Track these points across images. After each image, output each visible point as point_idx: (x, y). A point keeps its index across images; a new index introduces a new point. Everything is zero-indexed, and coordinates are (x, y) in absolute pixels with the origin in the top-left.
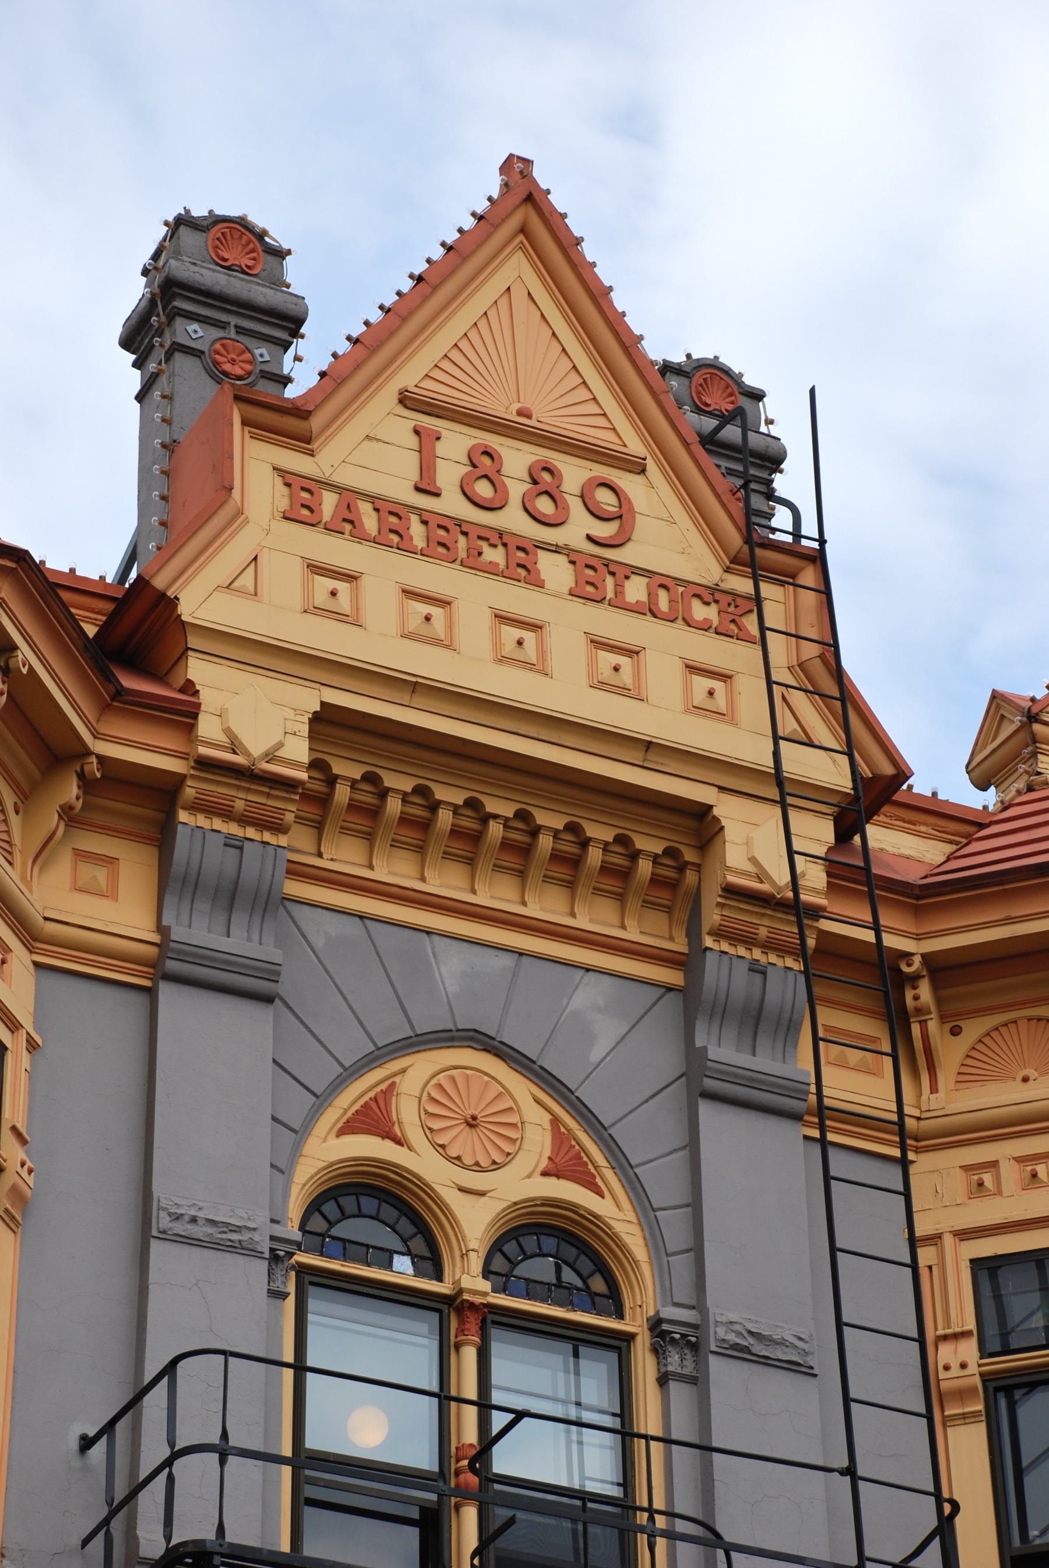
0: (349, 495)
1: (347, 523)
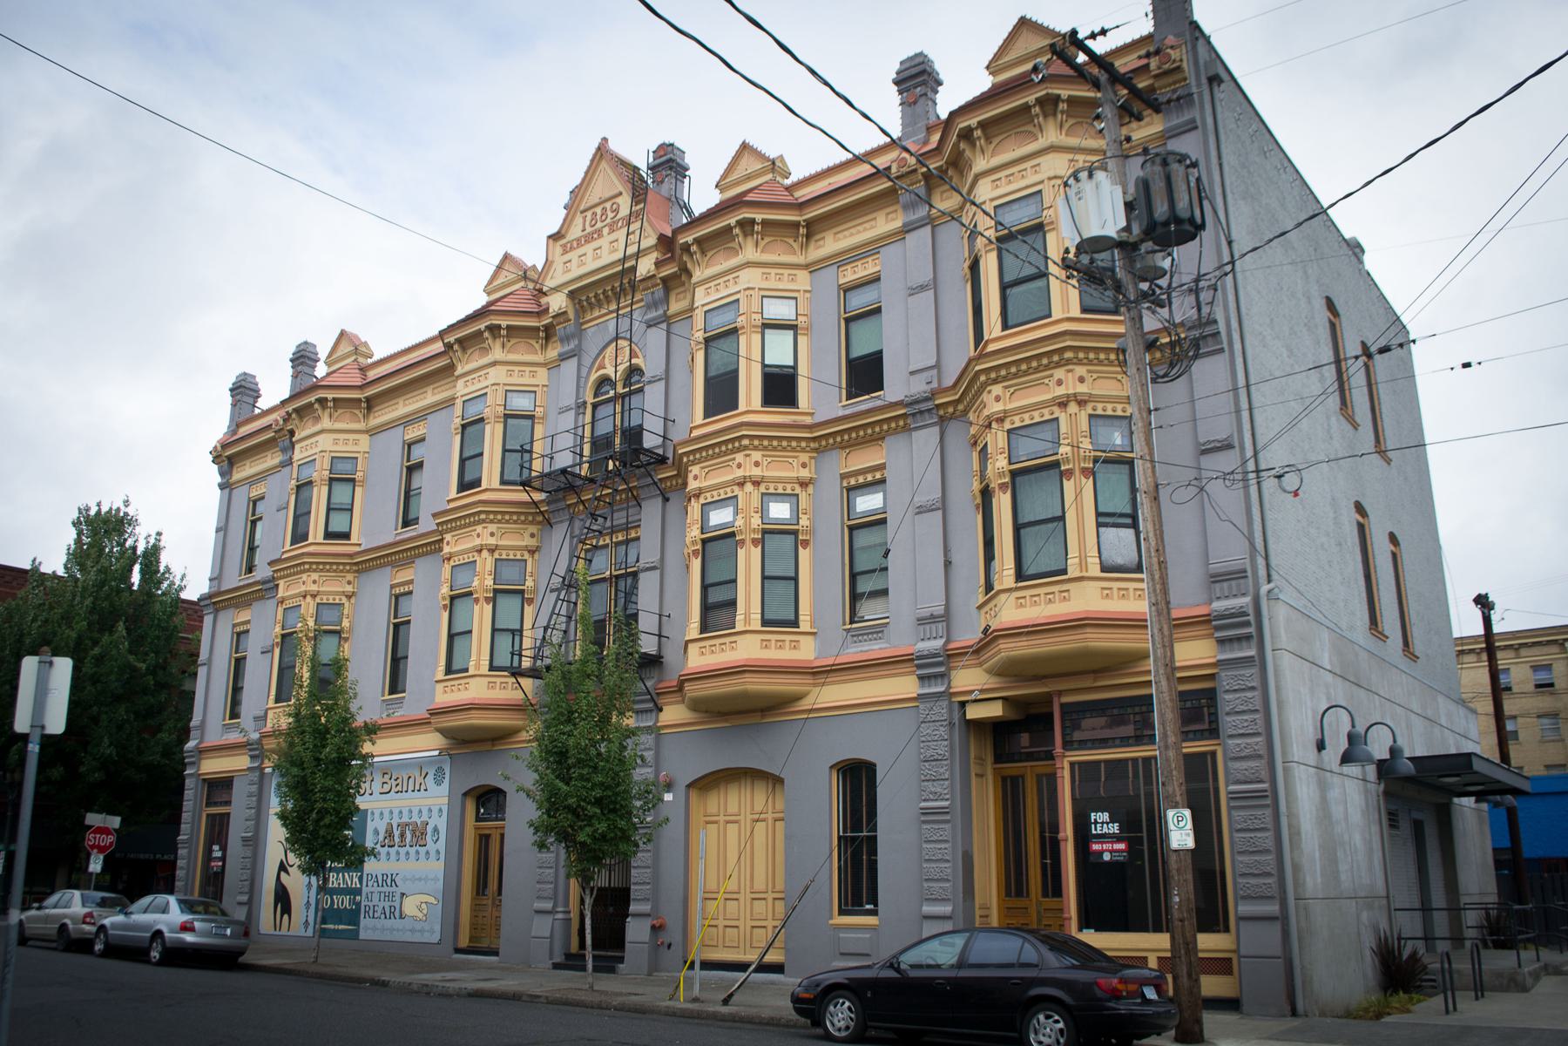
0: (578, 240)
1: (580, 245)
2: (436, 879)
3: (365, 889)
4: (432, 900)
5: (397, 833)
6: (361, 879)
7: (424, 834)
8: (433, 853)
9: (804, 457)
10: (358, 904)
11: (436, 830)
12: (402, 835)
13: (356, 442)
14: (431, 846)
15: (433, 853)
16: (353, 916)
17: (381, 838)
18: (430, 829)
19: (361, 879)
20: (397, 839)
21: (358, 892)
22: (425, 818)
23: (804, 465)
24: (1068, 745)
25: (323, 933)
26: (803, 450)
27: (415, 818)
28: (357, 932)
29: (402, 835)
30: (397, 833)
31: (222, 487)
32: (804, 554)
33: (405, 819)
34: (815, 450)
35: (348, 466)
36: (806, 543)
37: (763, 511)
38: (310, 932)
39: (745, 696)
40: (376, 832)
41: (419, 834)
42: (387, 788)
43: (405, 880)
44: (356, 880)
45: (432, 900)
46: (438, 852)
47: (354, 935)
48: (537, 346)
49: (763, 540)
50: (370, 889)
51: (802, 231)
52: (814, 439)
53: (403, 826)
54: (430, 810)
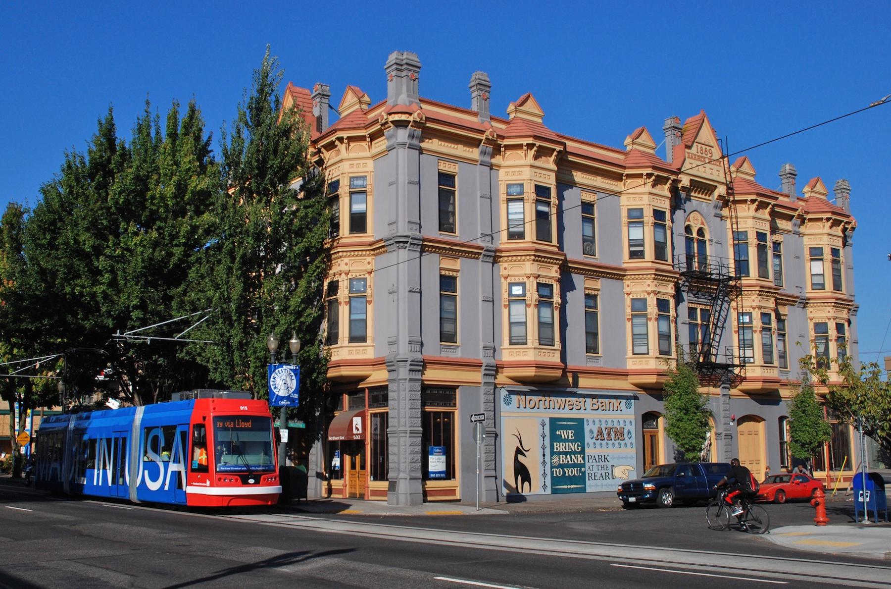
2: (632, 458)
3: (587, 465)
4: (631, 468)
5: (605, 433)
6: (584, 458)
7: (622, 434)
8: (629, 444)
9: (369, 259)
10: (584, 473)
11: (629, 432)
12: (609, 434)
13: (365, 165)
14: (627, 440)
15: (629, 444)
16: (581, 480)
17: (595, 435)
18: (625, 431)
19: (584, 458)
20: (606, 436)
21: (583, 465)
22: (622, 425)
23: (369, 263)
24: (370, 406)
25: (554, 491)
26: (368, 255)
27: (616, 425)
28: (585, 488)
29: (609, 434)
30: (605, 433)
31: (113, 125)
32: (369, 307)
33: (610, 425)
34: (374, 255)
35: (360, 182)
36: (370, 302)
37: (510, 291)
38: (549, 491)
39: (341, 377)
40: (591, 432)
41: (620, 434)
42: (595, 407)
43: (613, 458)
44: (580, 459)
45: (631, 468)
46: (632, 444)
47: (583, 490)
48: (367, 147)
49: (350, 302)
50: (591, 464)
51: (368, 140)
52: (373, 250)
53: (609, 430)
54: (600, 421)
